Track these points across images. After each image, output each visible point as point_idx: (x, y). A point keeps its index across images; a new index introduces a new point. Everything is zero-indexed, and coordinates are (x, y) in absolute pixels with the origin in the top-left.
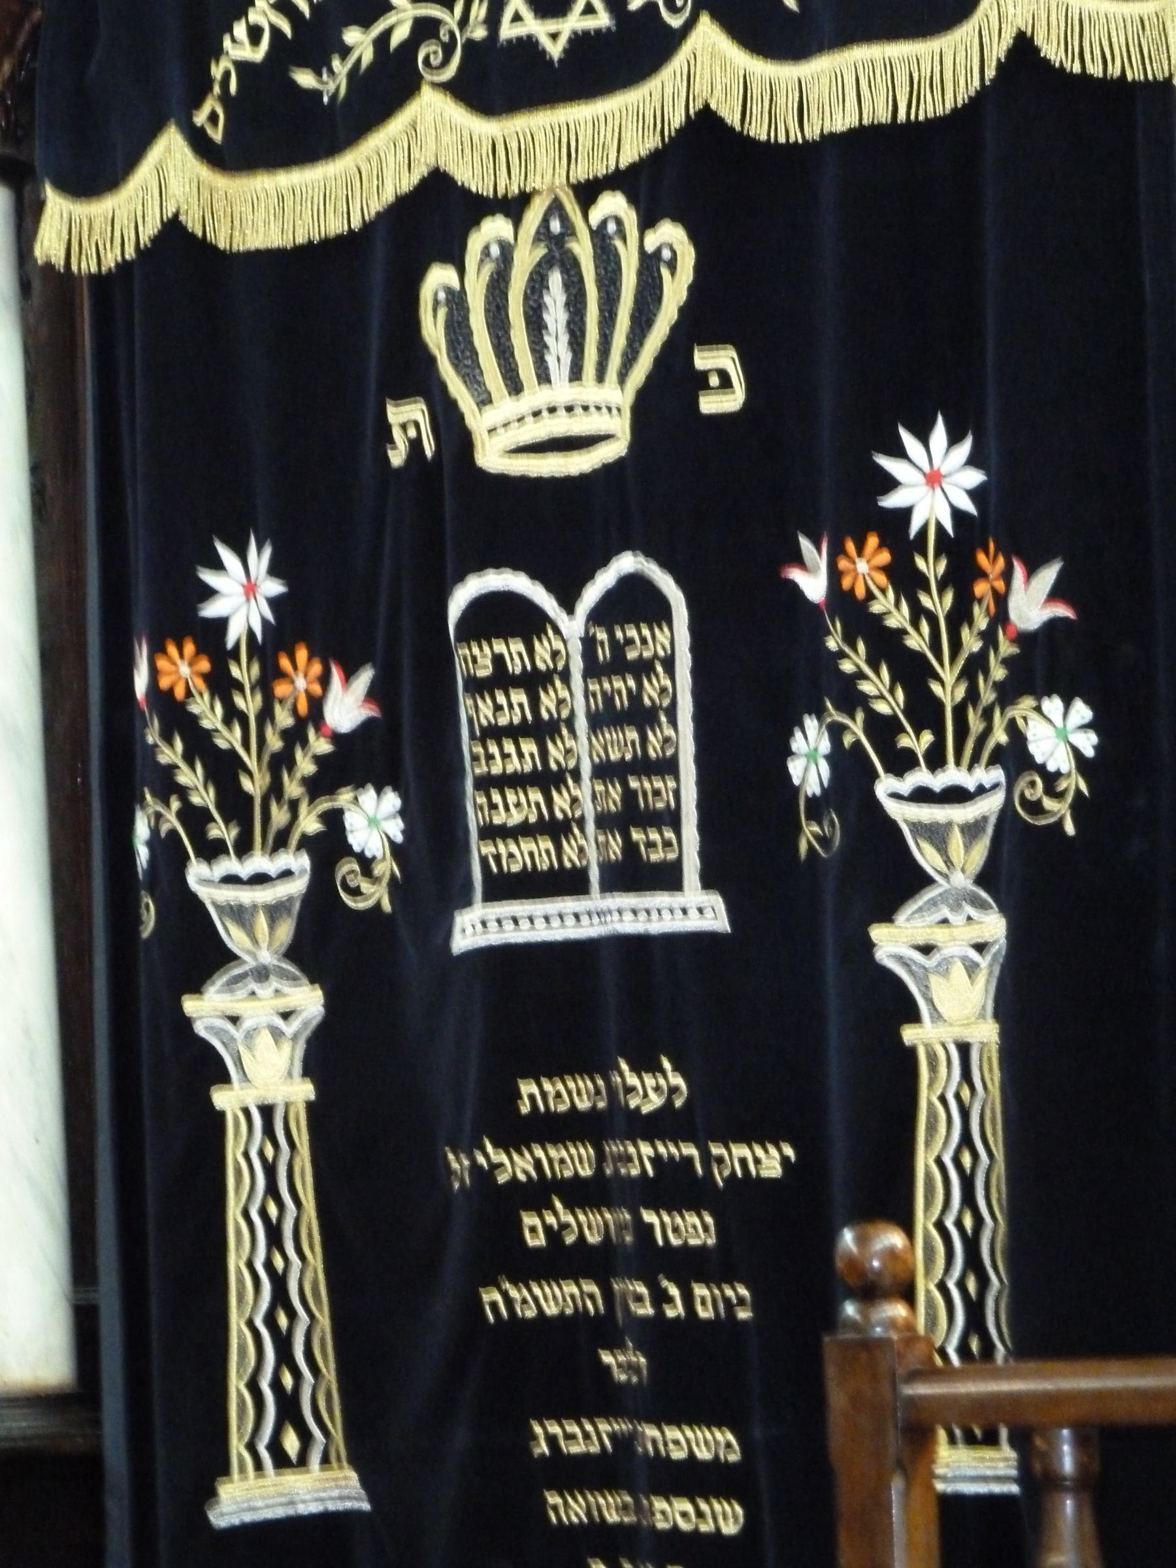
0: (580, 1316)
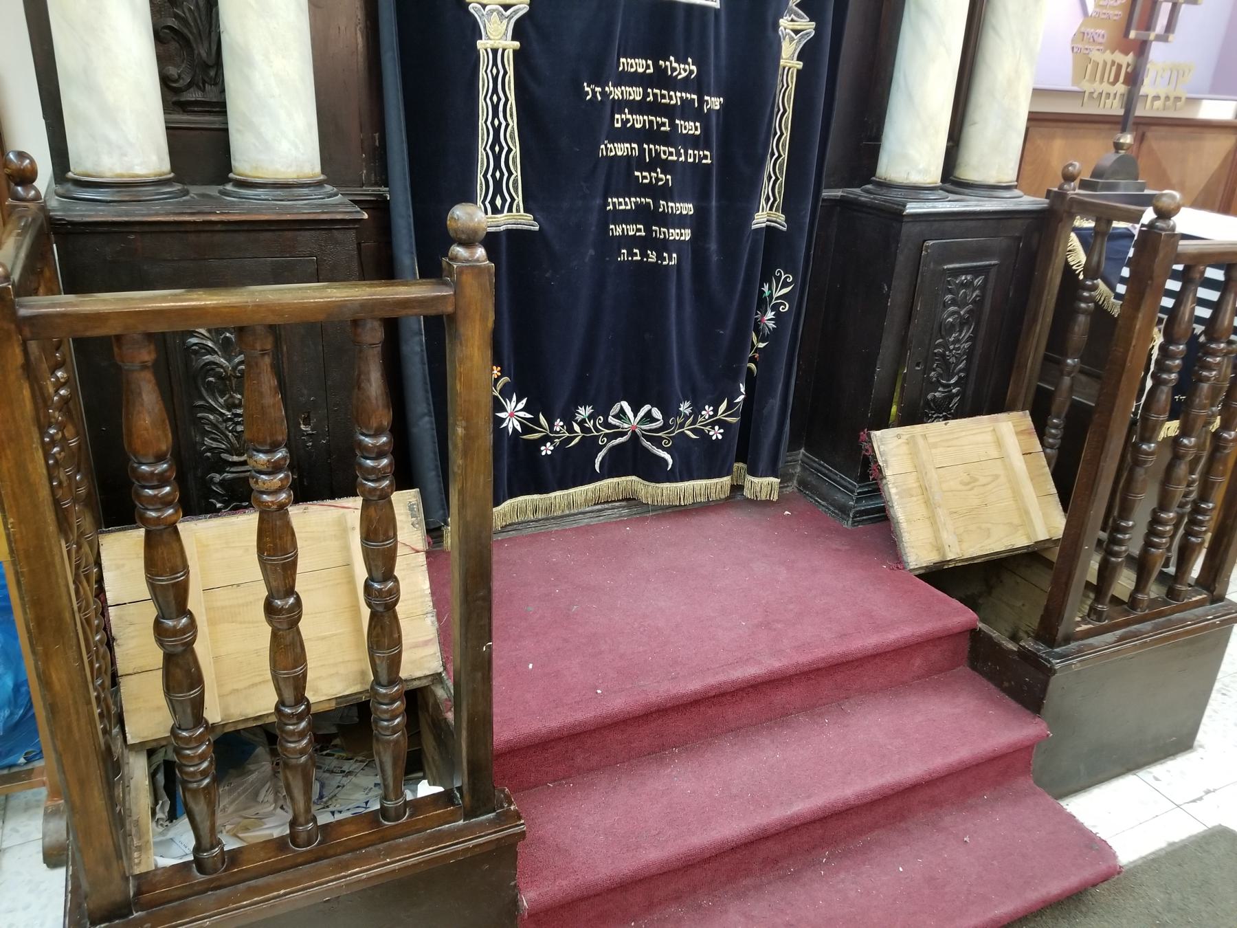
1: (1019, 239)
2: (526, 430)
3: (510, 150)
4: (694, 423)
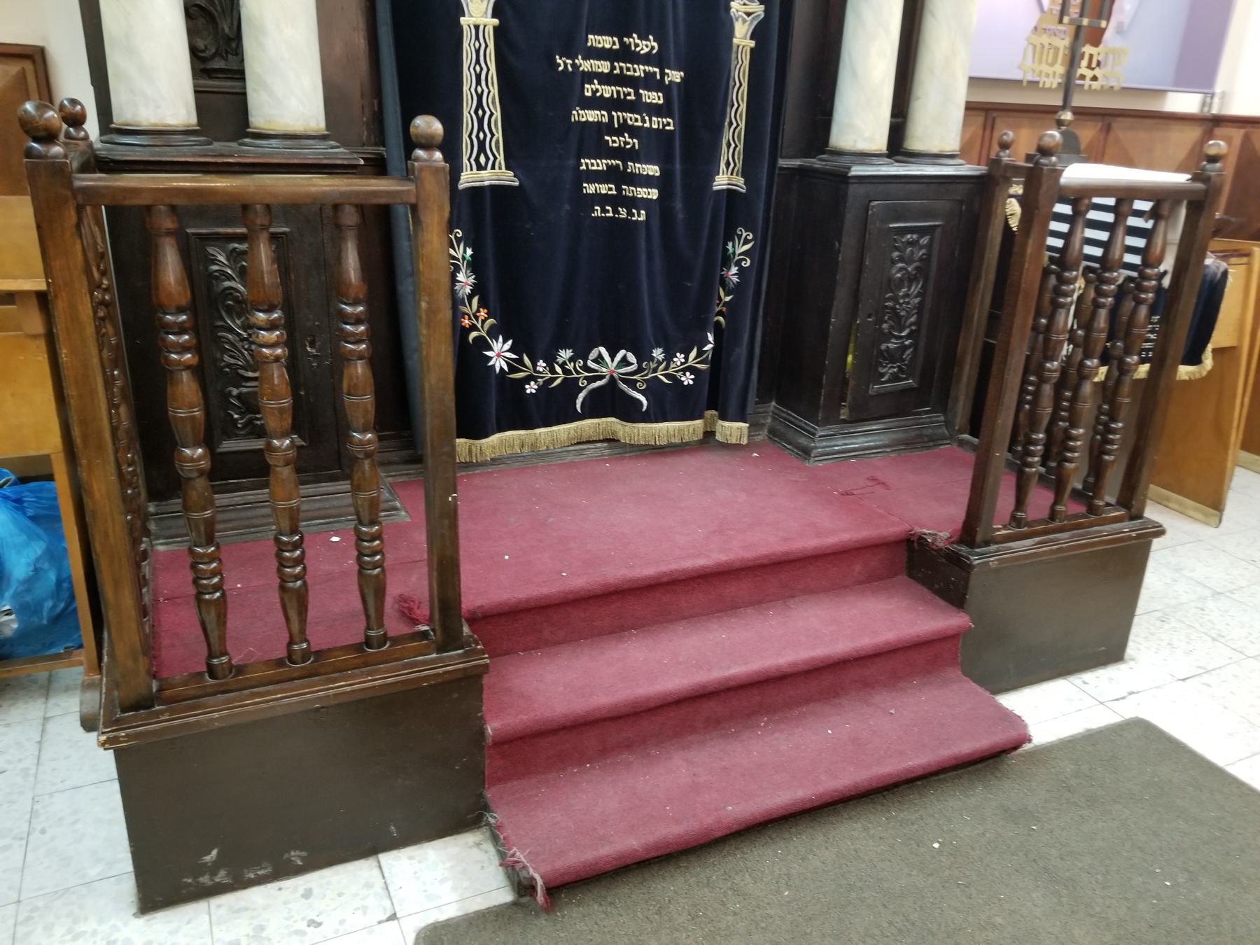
0: (599, 123)
1: (961, 202)
2: (513, 369)
3: (492, 114)
4: (666, 368)
